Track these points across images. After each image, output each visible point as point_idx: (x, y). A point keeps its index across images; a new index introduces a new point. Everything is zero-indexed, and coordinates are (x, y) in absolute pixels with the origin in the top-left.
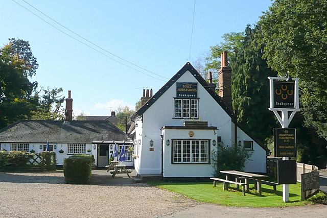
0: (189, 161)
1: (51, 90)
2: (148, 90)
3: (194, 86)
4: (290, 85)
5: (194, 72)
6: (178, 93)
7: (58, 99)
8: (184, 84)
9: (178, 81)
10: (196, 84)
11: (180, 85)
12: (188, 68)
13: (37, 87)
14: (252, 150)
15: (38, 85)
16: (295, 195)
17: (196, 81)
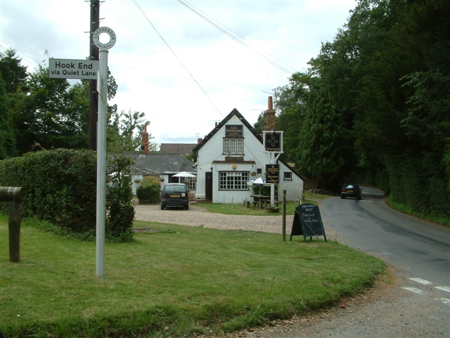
0: (221, 187)
1: (132, 114)
2: (5, 144)
3: (240, 127)
4: (277, 136)
5: (240, 116)
6: (227, 133)
7: (140, 124)
8: (232, 126)
9: (227, 124)
10: (226, 126)
11: (228, 127)
12: (235, 112)
13: (116, 109)
14: (292, 180)
15: (118, 108)
16: (192, 204)
17: (241, 123)
